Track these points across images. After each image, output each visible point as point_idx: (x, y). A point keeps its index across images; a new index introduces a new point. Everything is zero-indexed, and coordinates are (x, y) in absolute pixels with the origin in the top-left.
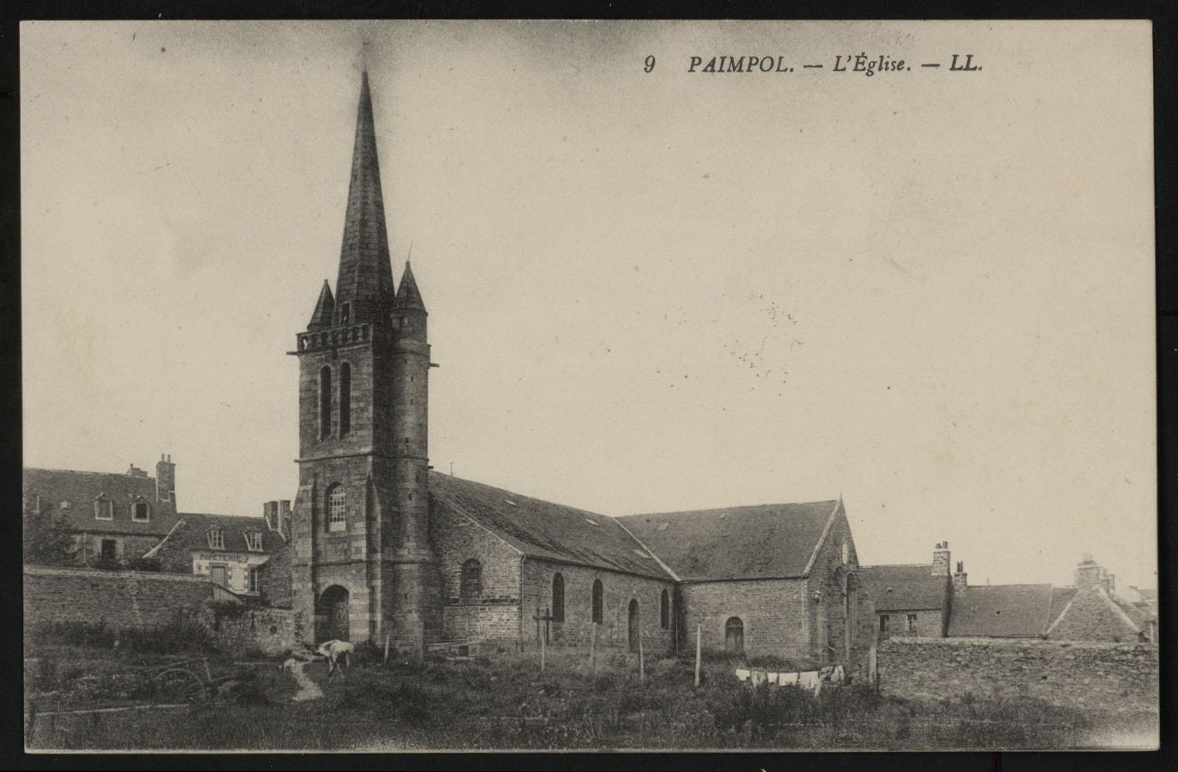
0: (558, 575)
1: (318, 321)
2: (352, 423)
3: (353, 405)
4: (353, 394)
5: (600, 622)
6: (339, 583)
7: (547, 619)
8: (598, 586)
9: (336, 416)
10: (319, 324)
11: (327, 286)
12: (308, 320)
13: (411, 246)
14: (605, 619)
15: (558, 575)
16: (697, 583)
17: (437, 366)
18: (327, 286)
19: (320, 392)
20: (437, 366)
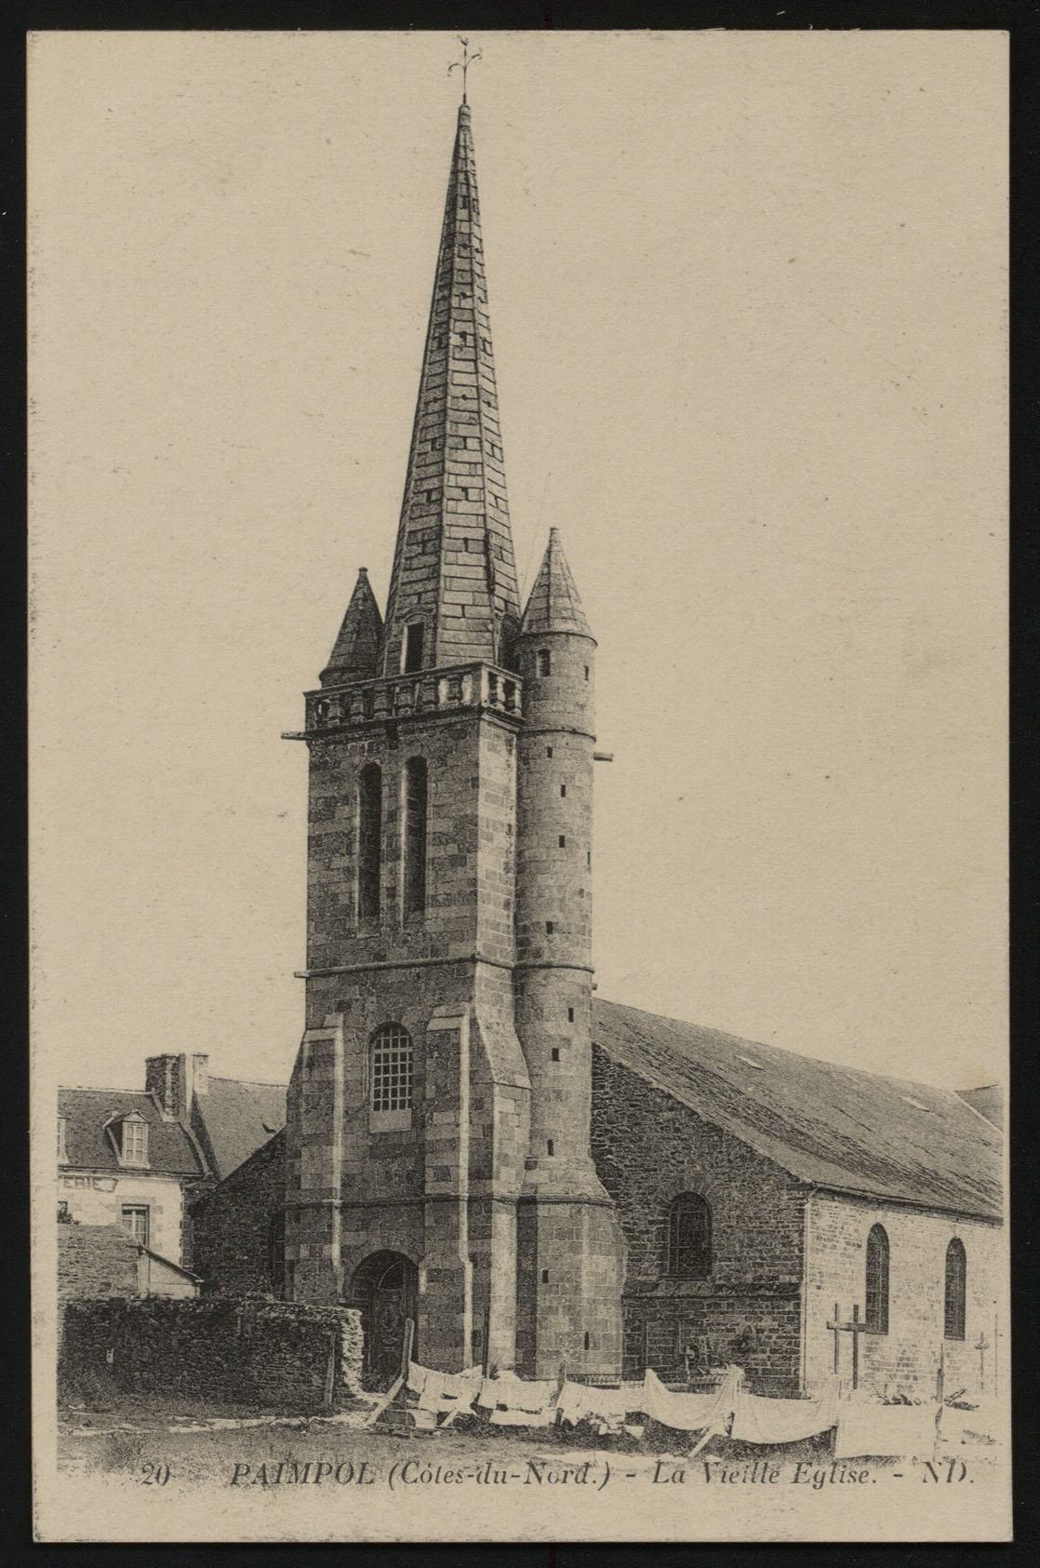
0: (878, 1229)
1: (341, 662)
2: (430, 890)
3: (431, 852)
4: (433, 825)
5: (960, 1334)
6: (395, 1246)
7: (854, 1328)
8: (878, 1241)
9: (396, 874)
10: (343, 670)
11: (363, 580)
12: (323, 662)
13: (551, 493)
14: (970, 1328)
15: (878, 1229)
16: (833, 1193)
17: (297, 976)
18: (363, 580)
19: (357, 821)
20: (297, 976)
